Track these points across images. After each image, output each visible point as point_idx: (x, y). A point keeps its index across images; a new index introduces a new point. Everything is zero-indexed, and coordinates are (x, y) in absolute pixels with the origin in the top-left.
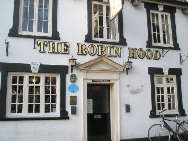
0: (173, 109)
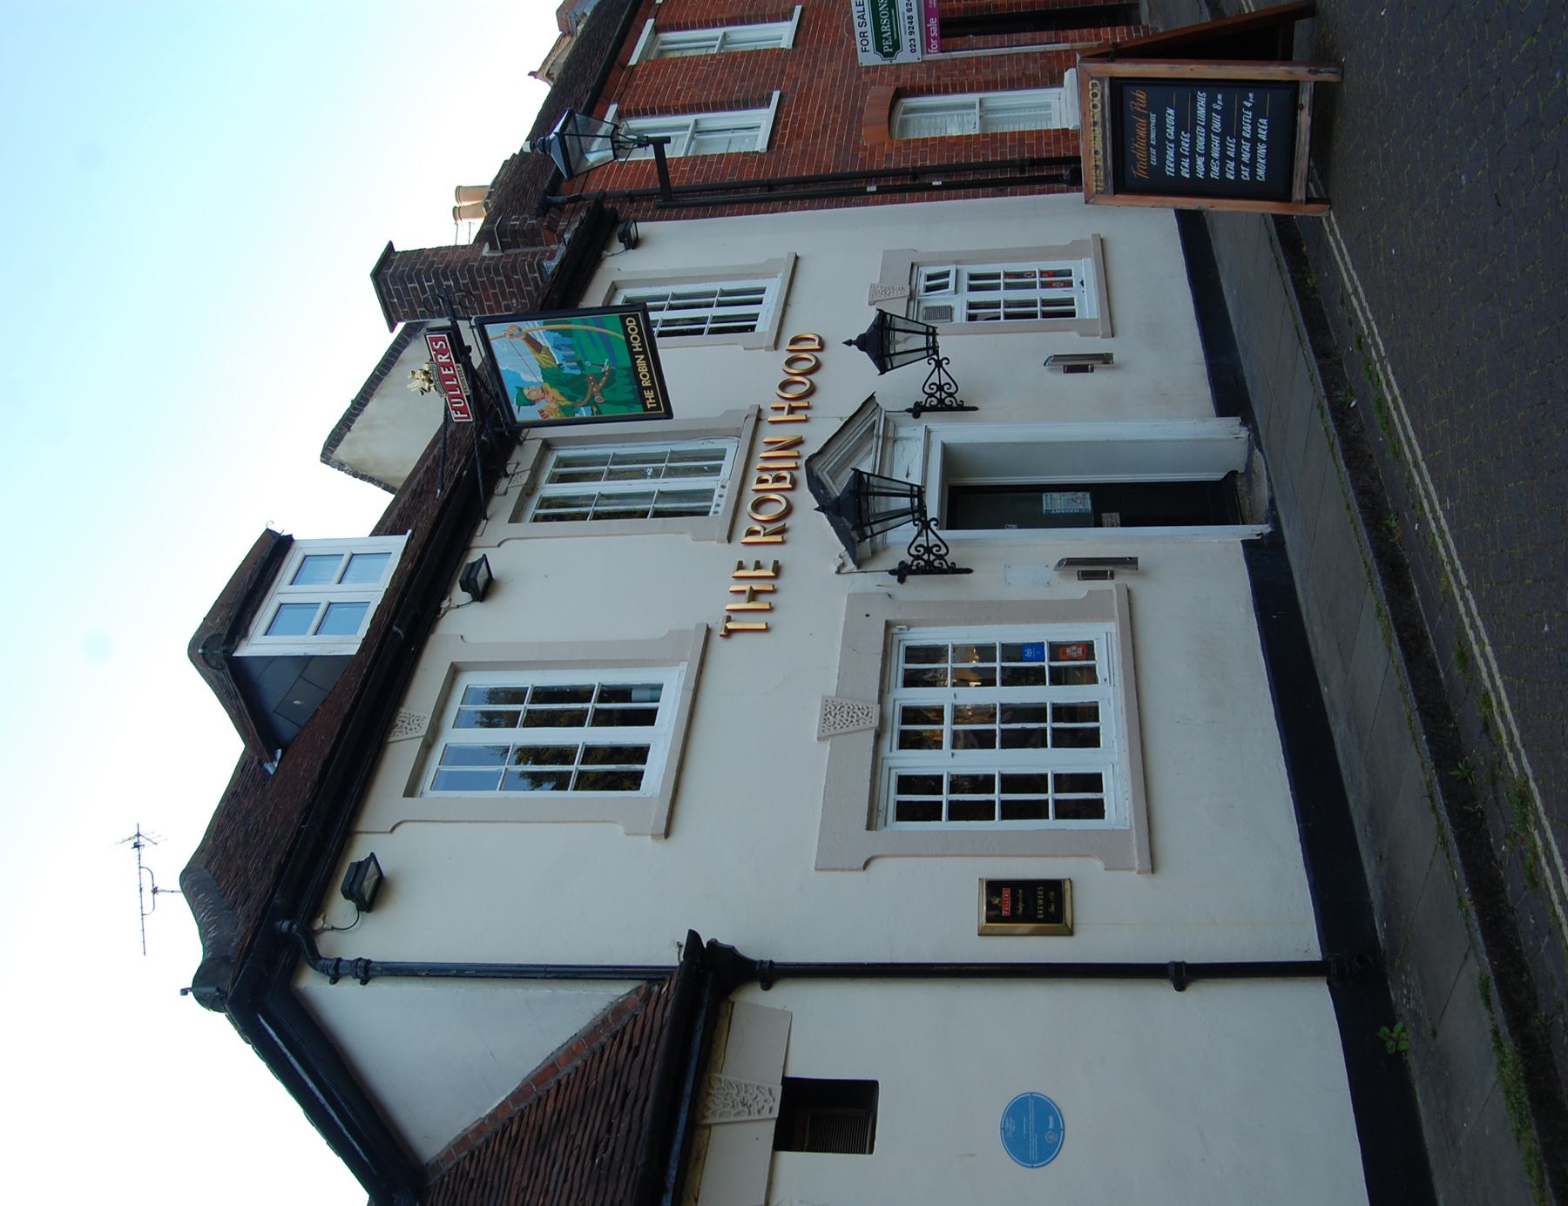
0: (1071, 275)
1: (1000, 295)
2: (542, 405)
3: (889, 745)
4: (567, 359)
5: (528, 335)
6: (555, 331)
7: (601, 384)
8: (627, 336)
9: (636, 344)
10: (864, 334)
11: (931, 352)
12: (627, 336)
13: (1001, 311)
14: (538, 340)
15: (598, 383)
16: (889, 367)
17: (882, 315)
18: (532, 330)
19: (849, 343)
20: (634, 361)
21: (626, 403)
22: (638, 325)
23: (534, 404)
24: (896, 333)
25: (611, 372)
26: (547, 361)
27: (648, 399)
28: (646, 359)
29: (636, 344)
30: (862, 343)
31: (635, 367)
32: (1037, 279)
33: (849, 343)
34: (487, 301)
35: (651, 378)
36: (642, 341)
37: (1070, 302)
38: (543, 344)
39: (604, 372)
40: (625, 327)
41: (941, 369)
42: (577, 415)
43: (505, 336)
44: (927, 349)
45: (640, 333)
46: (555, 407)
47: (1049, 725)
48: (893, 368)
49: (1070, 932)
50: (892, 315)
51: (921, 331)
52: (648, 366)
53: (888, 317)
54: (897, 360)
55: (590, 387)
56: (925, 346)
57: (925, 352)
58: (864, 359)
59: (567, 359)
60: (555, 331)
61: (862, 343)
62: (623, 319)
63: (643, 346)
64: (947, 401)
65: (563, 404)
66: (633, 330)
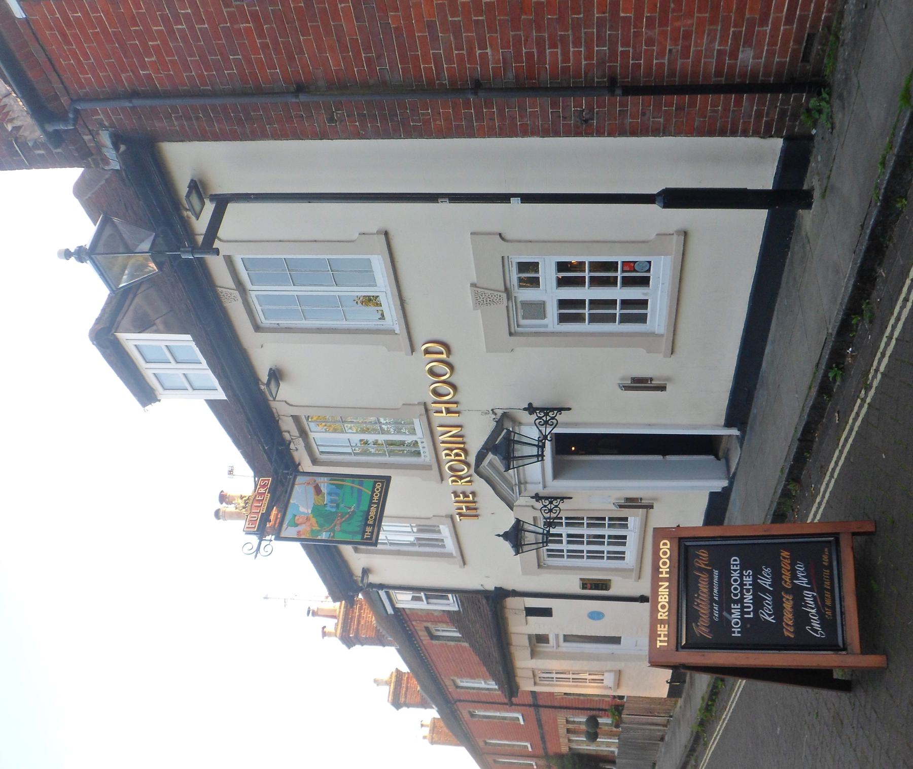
1: (585, 547)
2: (301, 528)
3: (314, 442)
4: (332, 501)
5: (317, 485)
6: (333, 484)
7: (343, 519)
8: (373, 492)
9: (376, 498)
10: (508, 532)
11: (540, 459)
12: (373, 492)
13: (587, 274)
14: (322, 489)
15: (342, 518)
16: (521, 552)
17: (518, 521)
18: (321, 483)
19: (499, 535)
20: (370, 507)
21: (354, 533)
22: (382, 488)
23: (297, 526)
24: (526, 532)
25: (354, 512)
26: (319, 501)
27: (367, 532)
28: (377, 508)
29: (376, 498)
30: (506, 536)
31: (369, 511)
32: (607, 522)
33: (499, 535)
34: (191, 56)
35: (375, 520)
36: (380, 497)
37: (624, 553)
38: (323, 491)
39: (349, 512)
40: (374, 487)
41: (544, 434)
42: (319, 538)
43: (304, 484)
44: (538, 456)
45: (380, 493)
46: (308, 530)
47: (586, 311)
48: (523, 552)
49: (581, 579)
50: (524, 522)
51: (536, 461)
52: (377, 512)
53: (522, 522)
54: (525, 548)
55: (336, 519)
56: (536, 454)
57: (542, 544)
58: (507, 546)
59: (332, 501)
60: (333, 484)
61: (506, 536)
62: (375, 483)
63: (379, 500)
64: (542, 414)
65: (314, 528)
66: (378, 490)
